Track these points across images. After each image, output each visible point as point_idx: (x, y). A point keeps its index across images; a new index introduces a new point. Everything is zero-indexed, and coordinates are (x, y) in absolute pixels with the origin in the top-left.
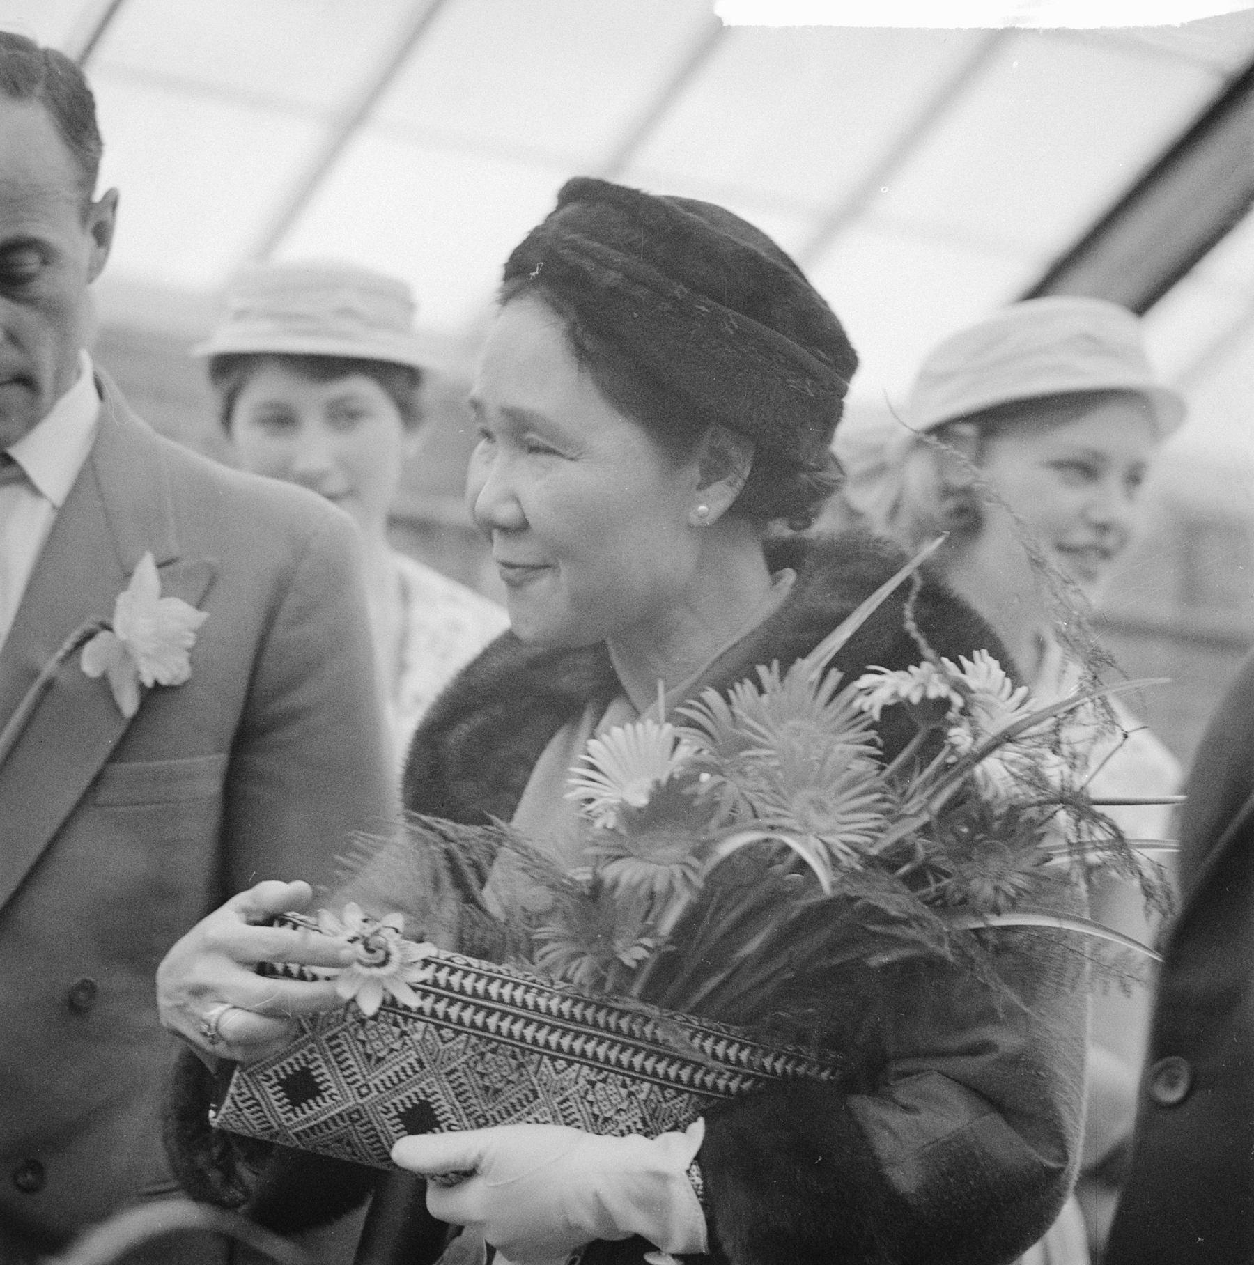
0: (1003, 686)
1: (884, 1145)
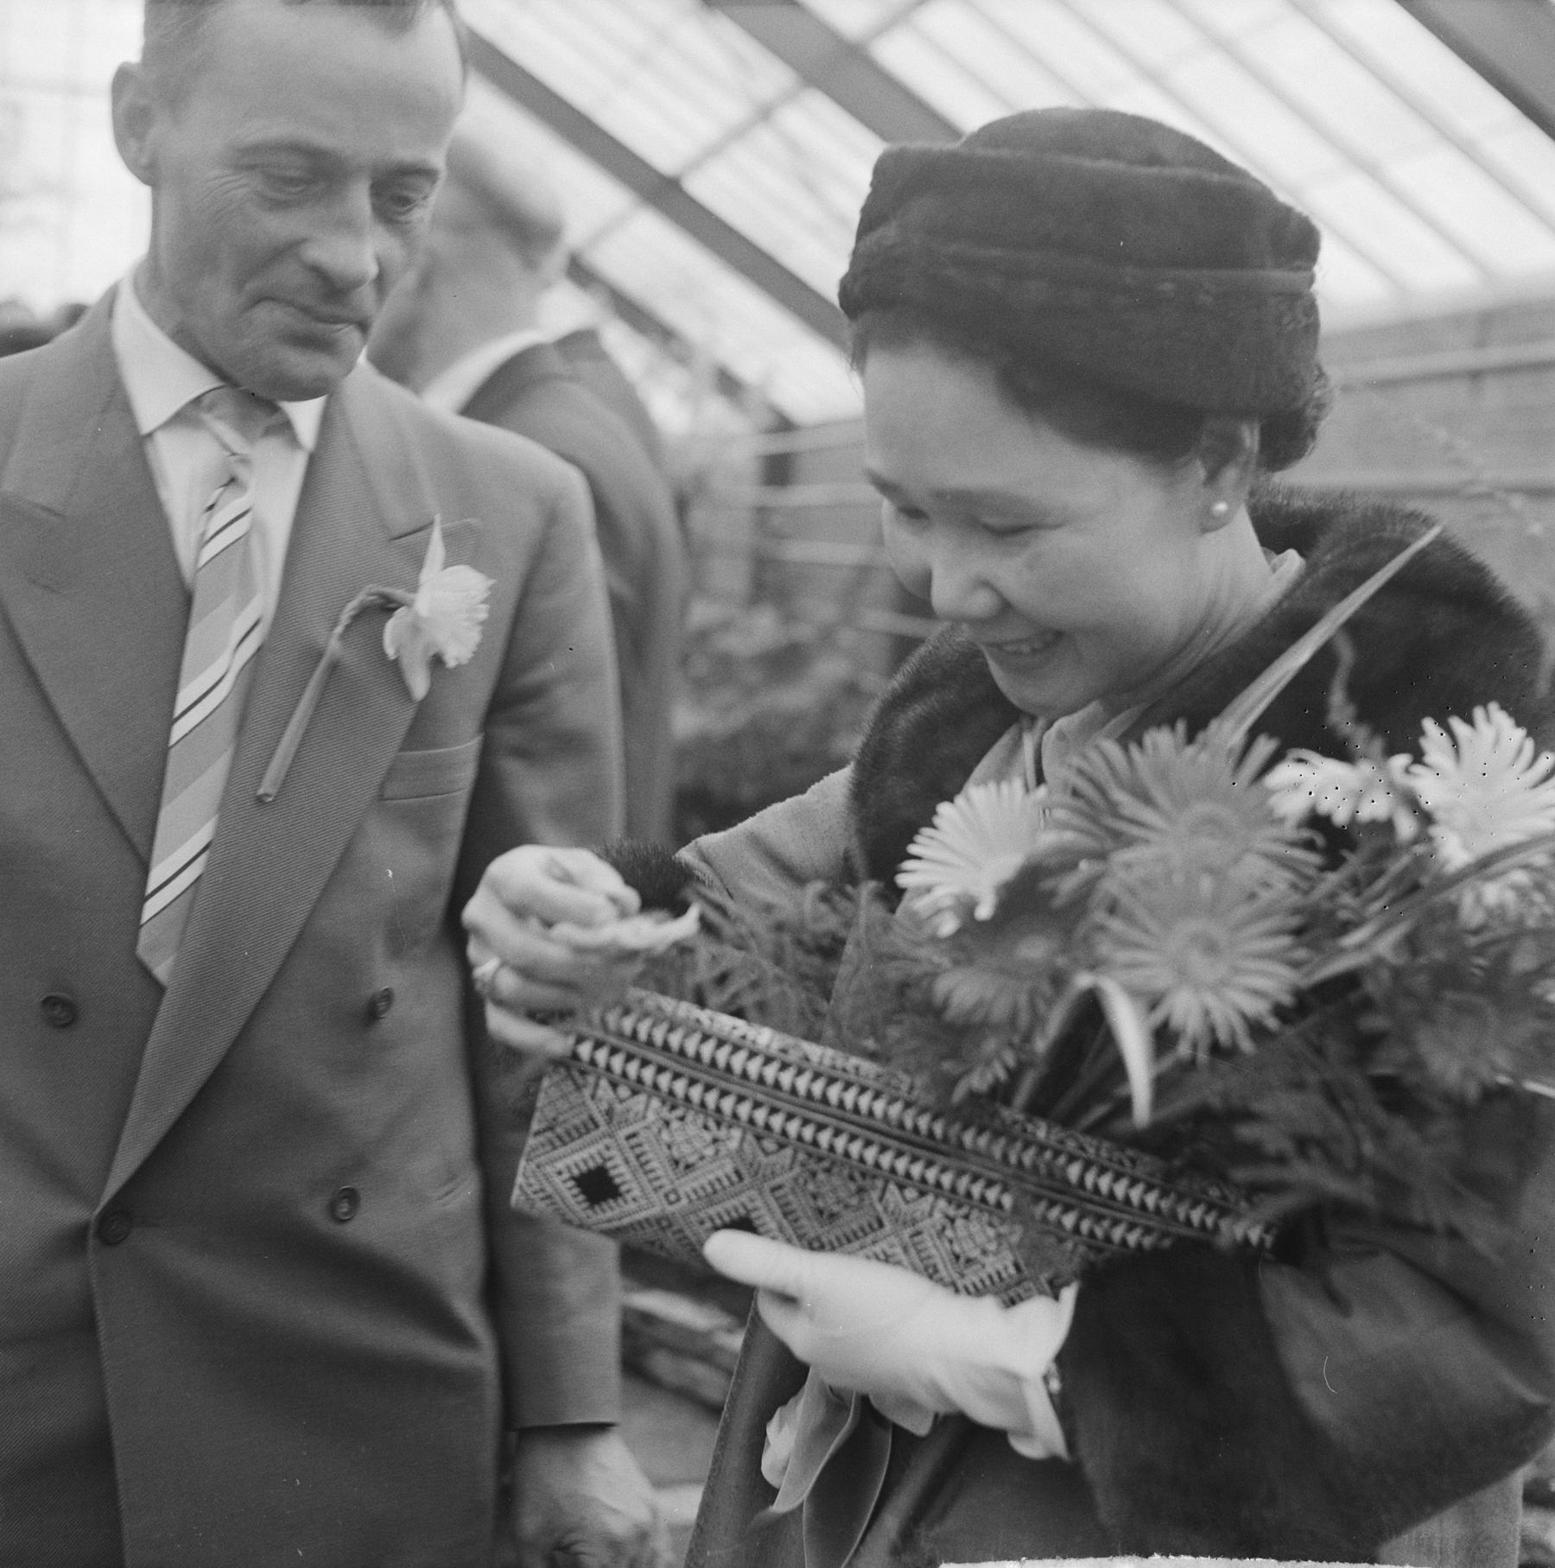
0: (1520, 751)
1: (1299, 1355)
